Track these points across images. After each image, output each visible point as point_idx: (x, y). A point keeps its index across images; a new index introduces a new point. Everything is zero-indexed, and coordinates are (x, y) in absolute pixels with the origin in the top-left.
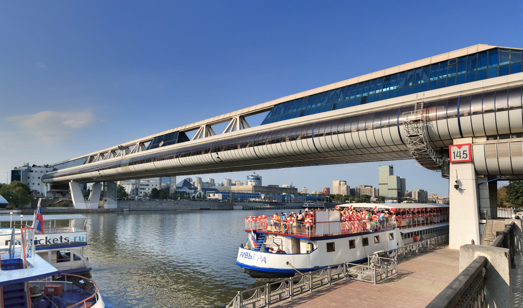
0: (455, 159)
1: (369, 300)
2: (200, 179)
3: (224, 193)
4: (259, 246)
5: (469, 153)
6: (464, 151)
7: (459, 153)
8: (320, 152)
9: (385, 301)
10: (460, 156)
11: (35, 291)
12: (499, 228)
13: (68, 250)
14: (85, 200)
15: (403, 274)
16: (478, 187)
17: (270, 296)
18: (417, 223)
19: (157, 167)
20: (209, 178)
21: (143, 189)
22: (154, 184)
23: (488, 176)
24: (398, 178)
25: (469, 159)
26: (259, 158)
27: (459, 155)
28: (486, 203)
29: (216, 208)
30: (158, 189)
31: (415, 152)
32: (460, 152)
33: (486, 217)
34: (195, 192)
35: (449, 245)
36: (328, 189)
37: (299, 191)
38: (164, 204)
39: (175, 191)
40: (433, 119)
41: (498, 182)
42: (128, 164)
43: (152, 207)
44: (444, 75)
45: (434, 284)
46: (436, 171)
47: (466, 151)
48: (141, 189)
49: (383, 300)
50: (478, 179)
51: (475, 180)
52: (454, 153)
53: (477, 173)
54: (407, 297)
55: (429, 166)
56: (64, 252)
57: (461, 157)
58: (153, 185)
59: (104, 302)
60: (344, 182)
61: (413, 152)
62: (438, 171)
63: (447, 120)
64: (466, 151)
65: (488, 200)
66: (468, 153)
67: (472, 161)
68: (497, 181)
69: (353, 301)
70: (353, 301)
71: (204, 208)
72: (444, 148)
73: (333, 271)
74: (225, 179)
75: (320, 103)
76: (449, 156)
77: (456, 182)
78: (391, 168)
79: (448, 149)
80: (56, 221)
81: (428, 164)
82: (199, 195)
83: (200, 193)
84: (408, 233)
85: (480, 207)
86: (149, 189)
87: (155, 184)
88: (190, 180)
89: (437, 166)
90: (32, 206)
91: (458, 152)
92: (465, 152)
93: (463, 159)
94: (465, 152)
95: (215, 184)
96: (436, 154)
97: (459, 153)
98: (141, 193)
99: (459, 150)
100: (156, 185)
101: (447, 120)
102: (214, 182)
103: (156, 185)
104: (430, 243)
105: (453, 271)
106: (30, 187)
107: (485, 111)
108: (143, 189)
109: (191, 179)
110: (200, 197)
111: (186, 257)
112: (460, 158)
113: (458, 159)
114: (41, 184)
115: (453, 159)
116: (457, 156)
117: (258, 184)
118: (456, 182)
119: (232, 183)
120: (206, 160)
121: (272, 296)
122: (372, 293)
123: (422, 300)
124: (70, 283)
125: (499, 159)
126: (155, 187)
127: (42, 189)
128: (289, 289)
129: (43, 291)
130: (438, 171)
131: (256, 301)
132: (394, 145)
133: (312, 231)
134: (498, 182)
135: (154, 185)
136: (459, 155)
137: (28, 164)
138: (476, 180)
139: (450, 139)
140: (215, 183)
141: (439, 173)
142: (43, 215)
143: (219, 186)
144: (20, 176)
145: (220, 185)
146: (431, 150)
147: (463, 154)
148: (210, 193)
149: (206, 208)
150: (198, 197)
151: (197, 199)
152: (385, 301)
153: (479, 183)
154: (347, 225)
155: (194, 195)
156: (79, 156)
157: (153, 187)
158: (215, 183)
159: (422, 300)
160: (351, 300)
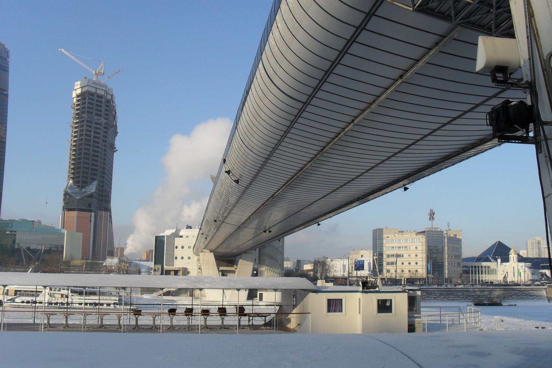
2: (83, 303)
11: (25, 249)
12: (251, 209)
13: (227, 302)
14: (178, 275)
18: (122, 331)
25: (521, 251)
33: (418, 283)
37: (56, 228)
40: (199, 272)
42: (487, 304)
44: (517, 141)
48: (388, 264)
56: (76, 90)
58: (410, 263)
59: (495, 68)
63: (423, 307)
75: (267, 322)
80: (347, 284)
84: (330, 312)
87: (414, 261)
90: (50, 324)
98: (388, 271)
101: (423, 307)
104: (480, 285)
107: (369, 272)
111: (92, 314)
114: (192, 258)
124: (547, 266)
127: (193, 262)
128: (453, 274)
133: (88, 305)
137: (73, 118)
139: (376, 14)
142: (531, 105)
144: (164, 241)
154: (425, 295)
156: (443, 271)
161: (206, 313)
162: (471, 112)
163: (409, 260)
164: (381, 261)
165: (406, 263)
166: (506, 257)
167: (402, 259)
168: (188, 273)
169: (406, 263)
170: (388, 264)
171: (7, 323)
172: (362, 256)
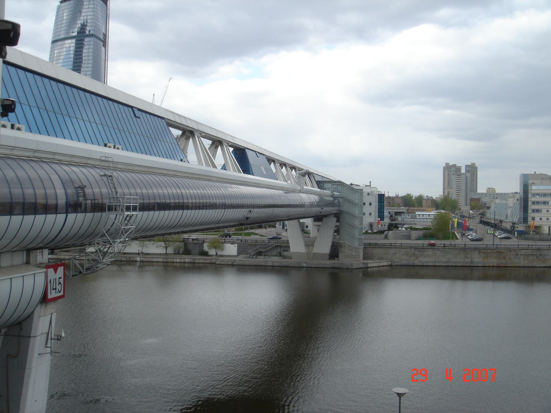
3: (315, 217)
4: (348, 214)
7: (55, 279)
15: (325, 216)
21: (538, 211)
22: (543, 216)
35: (92, 78)
48: (534, 211)
68: (236, 254)
73: (303, 197)
91: (54, 279)
97: (55, 279)
106: (55, 304)
108: (538, 211)
132: (88, 121)
161: (426, 204)
162: (36, 162)
163: (547, 215)
164: (527, 202)
165: (544, 219)
166: (79, 42)
167: (547, 206)
168: (369, 193)
169: (544, 219)
170: (534, 211)
171: (535, 204)
172: (235, 246)
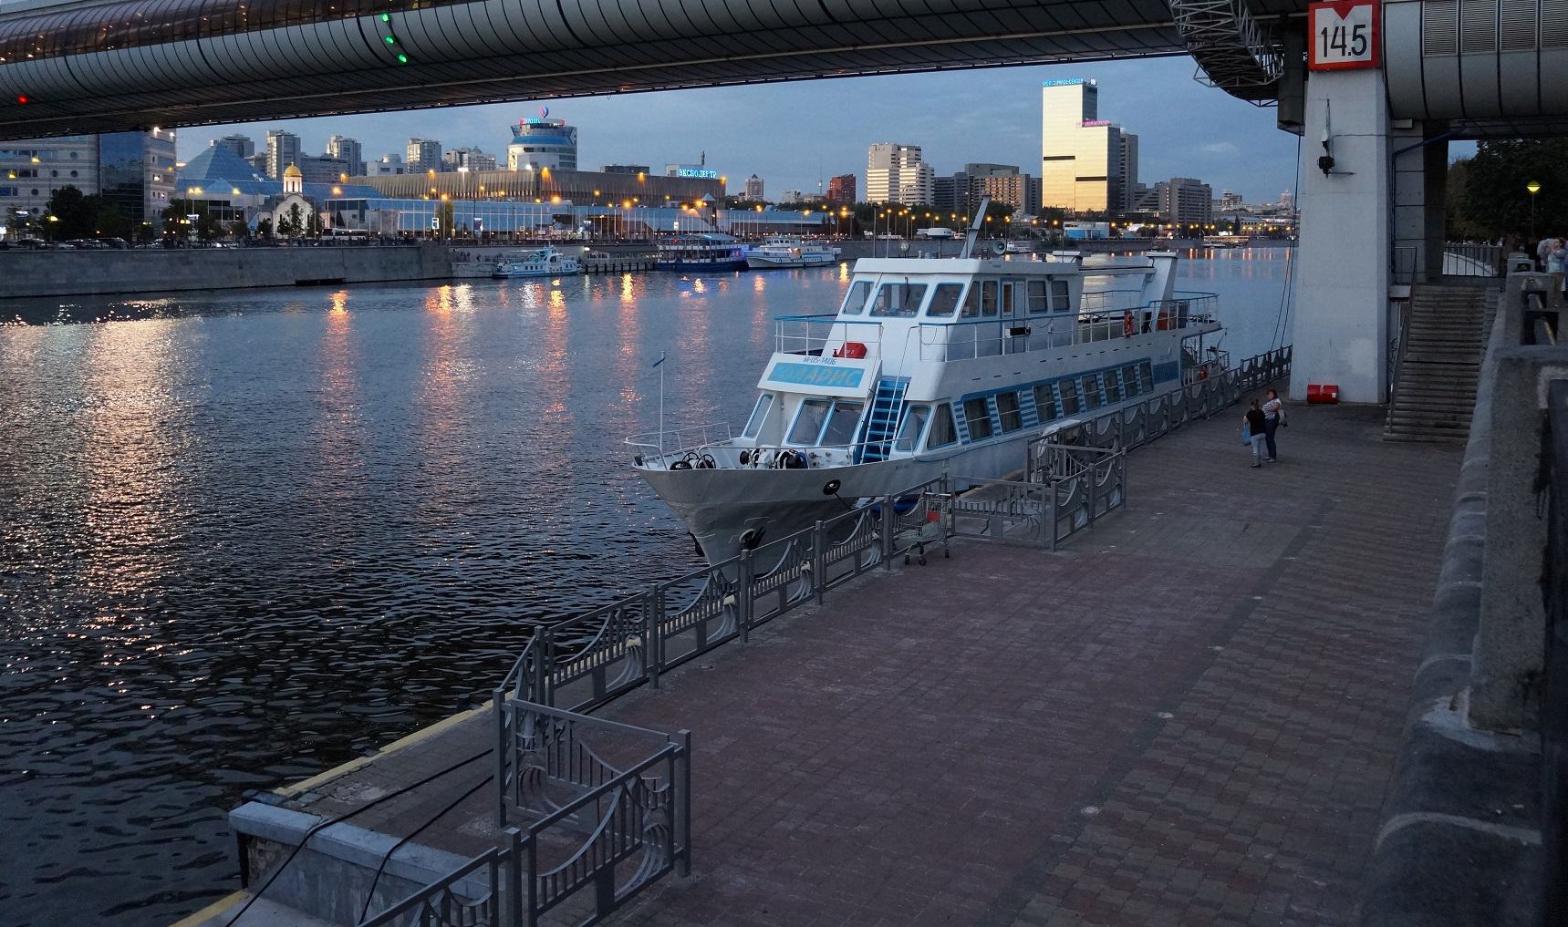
0: (1325, 55)
1: (1036, 611)
5: (1374, 34)
6: (1356, 27)
7: (1340, 32)
8: (839, 20)
9: (1093, 608)
10: (1343, 46)
16: (1394, 163)
17: (664, 637)
19: (215, 64)
20: (334, 138)
23: (1424, 122)
24: (1113, 133)
26: (582, 46)
27: (1339, 41)
28: (1415, 223)
29: (373, 274)
30: (86, 192)
31: (1192, 29)
32: (1343, 28)
34: (271, 205)
36: (848, 184)
38: (120, 265)
39: (172, 201)
41: (1452, 144)
43: (58, 282)
45: (1247, 530)
46: (1257, 102)
47: (1363, 26)
49: (1084, 605)
50: (1396, 133)
51: (1384, 138)
52: (1325, 32)
53: (1393, 111)
54: (1165, 589)
55: (1237, 85)
57: (1348, 50)
60: (913, 153)
61: (1187, 27)
62: (1263, 102)
64: (1363, 26)
65: (1421, 212)
66: (1367, 32)
67: (1378, 62)
69: (979, 623)
70: (979, 623)
71: (314, 278)
72: (1291, 15)
74: (413, 140)
76: (1306, 44)
77: (1325, 144)
78: (1090, 92)
79: (1306, 18)
81: (1234, 75)
82: (288, 219)
83: (295, 207)
85: (1395, 240)
86: (35, 192)
87: (68, 168)
88: (242, 146)
89: (1265, 83)
92: (1359, 31)
93: (1353, 58)
94: (1359, 31)
95: (364, 165)
96: (1262, 40)
97: (1340, 32)
99: (1341, 23)
100: (74, 173)
102: (357, 155)
103: (74, 173)
105: (1306, 478)
109: (247, 139)
110: (295, 226)
112: (1343, 54)
113: (1335, 57)
115: (1320, 59)
116: (1333, 47)
117: (561, 164)
118: (1325, 144)
119: (444, 157)
120: (194, 67)
121: (671, 635)
122: (1043, 584)
123: (1214, 593)
125: (1541, 54)
126: (68, 183)
129: (593, 911)
130: (1264, 106)
131: (606, 664)
132: (1009, 8)
134: (1452, 144)
135: (65, 174)
136: (1339, 41)
138: (1387, 136)
140: (363, 160)
141: (1266, 114)
143: (384, 175)
145: (388, 170)
146: (1250, 21)
147: (1354, 40)
148: (344, 208)
149: (324, 278)
150: (284, 228)
151: (280, 236)
152: (1093, 608)
153: (1396, 150)
155: (265, 216)
157: (59, 184)
158: (363, 160)
159: (1214, 593)
160: (972, 620)
